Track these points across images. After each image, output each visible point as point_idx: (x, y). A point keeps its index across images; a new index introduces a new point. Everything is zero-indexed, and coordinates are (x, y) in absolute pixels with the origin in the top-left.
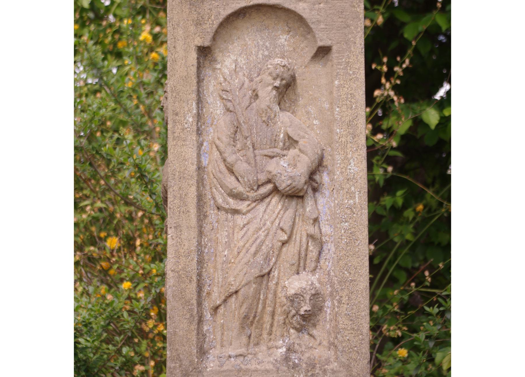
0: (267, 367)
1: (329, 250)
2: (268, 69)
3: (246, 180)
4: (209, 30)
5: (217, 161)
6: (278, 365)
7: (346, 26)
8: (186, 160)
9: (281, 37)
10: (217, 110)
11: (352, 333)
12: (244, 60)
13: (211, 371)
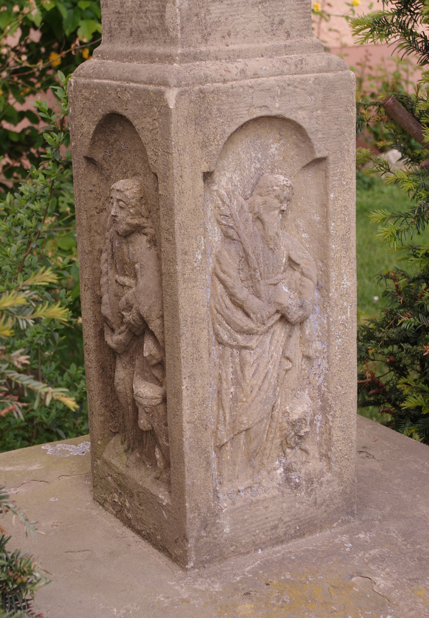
0: (274, 494)
1: (319, 366)
2: (274, 190)
3: (259, 316)
4: (215, 152)
5: (222, 296)
6: (282, 488)
7: (341, 133)
8: (196, 303)
9: (272, 146)
10: (215, 237)
11: (343, 443)
12: (238, 177)
13: (226, 511)
